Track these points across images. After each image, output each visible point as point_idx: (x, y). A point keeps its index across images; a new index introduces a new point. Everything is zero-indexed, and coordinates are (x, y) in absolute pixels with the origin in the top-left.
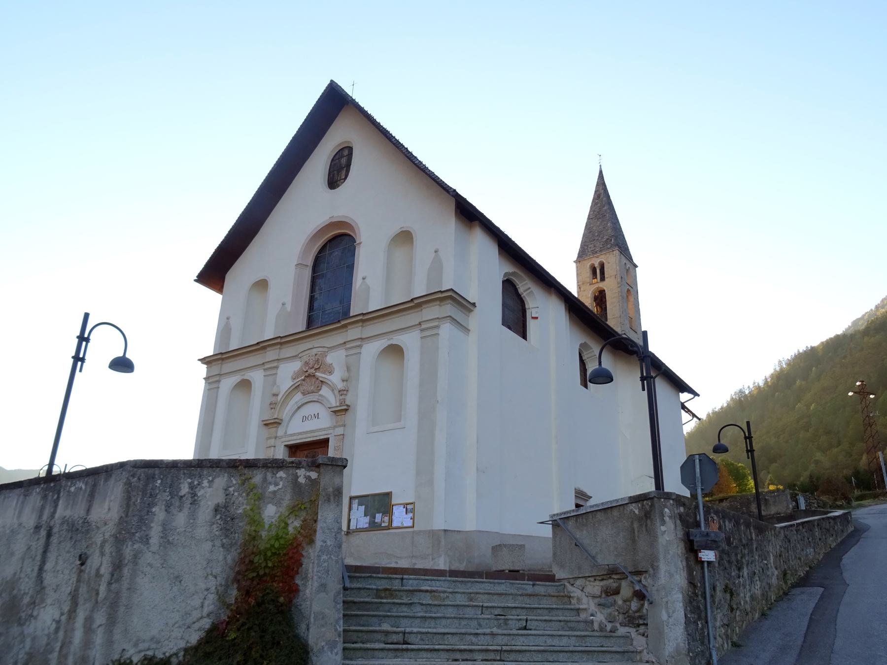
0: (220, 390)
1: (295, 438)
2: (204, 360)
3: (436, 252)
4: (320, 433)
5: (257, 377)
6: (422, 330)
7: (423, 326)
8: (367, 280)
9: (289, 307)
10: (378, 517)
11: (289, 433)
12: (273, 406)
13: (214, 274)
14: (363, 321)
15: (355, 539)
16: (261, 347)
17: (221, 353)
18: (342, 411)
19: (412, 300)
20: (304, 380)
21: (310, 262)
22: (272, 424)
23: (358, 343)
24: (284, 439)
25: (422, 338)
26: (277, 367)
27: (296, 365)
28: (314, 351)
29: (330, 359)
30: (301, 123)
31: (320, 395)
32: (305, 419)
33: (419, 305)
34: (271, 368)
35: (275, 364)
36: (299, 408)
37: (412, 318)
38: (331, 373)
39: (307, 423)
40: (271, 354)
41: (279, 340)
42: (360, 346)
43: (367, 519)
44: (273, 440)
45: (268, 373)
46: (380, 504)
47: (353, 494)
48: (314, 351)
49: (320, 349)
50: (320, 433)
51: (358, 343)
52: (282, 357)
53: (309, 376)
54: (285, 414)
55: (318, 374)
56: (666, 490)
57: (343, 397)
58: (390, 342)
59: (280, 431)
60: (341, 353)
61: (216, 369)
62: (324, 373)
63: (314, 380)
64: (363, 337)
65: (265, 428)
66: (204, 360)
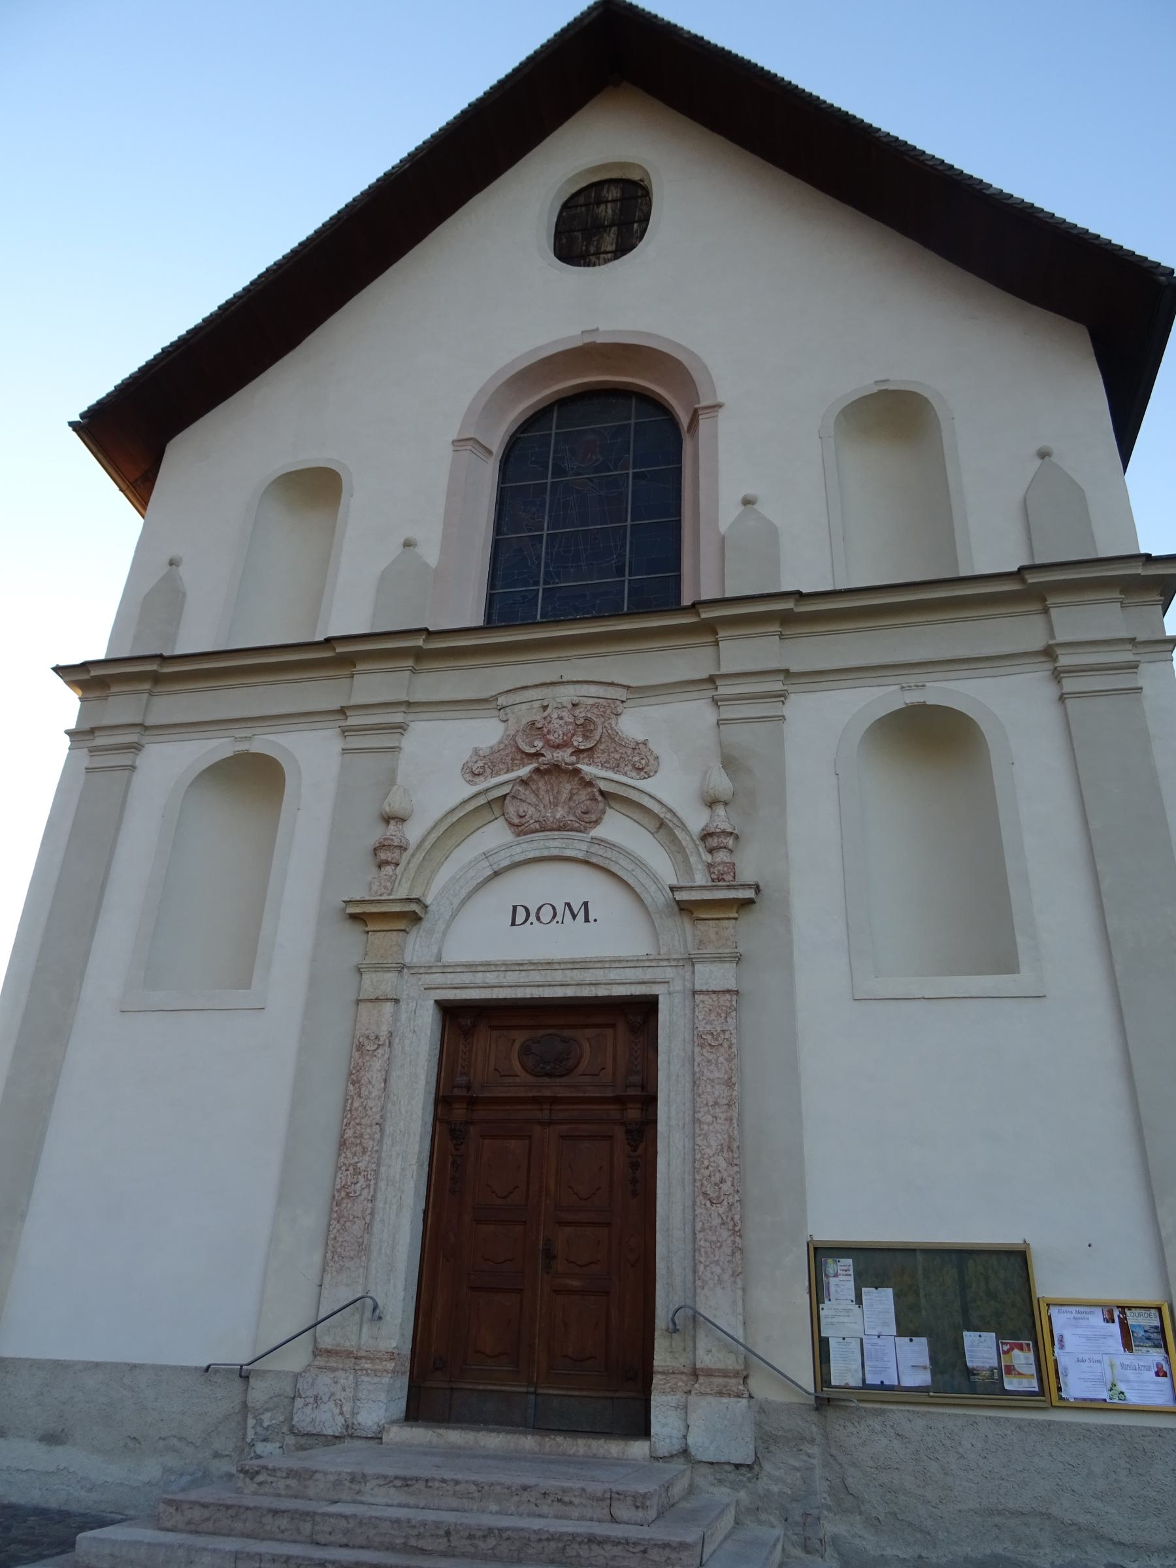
0: (138, 779)
1: (491, 978)
2: (78, 675)
3: (171, 563)
4: (613, 975)
5: (312, 757)
6: (345, 732)
7: (353, 720)
8: (761, 508)
9: (430, 553)
10: (980, 1349)
11: (448, 958)
12: (384, 855)
13: (135, 429)
14: (419, 655)
15: (869, 1439)
16: (337, 655)
17: (161, 658)
18: (722, 905)
19: (328, 641)
20: (524, 782)
21: (497, 442)
22: (383, 918)
23: (131, 737)
24: (428, 979)
25: (89, 770)
26: (401, 728)
27: (487, 732)
28: (567, 694)
29: (632, 725)
30: (502, 75)
31: (600, 842)
32: (519, 915)
33: (347, 662)
34: (373, 733)
35: (398, 718)
36: (496, 874)
37: (320, 693)
38: (643, 771)
39: (545, 926)
40: (372, 685)
41: (419, 642)
42: (136, 747)
43: (917, 1351)
44: (391, 976)
45: (356, 742)
46: (971, 1296)
47: (828, 1233)
48: (567, 694)
49: (593, 690)
50: (613, 975)
51: (131, 737)
52: (357, 700)
53: (555, 769)
54: (438, 888)
55: (588, 769)
56: (890, 1291)
57: (722, 856)
58: (913, 698)
59: (416, 947)
60: (697, 713)
61: (123, 707)
62: (616, 768)
63: (567, 787)
64: (794, 668)
65: (349, 926)
66: (68, 732)
